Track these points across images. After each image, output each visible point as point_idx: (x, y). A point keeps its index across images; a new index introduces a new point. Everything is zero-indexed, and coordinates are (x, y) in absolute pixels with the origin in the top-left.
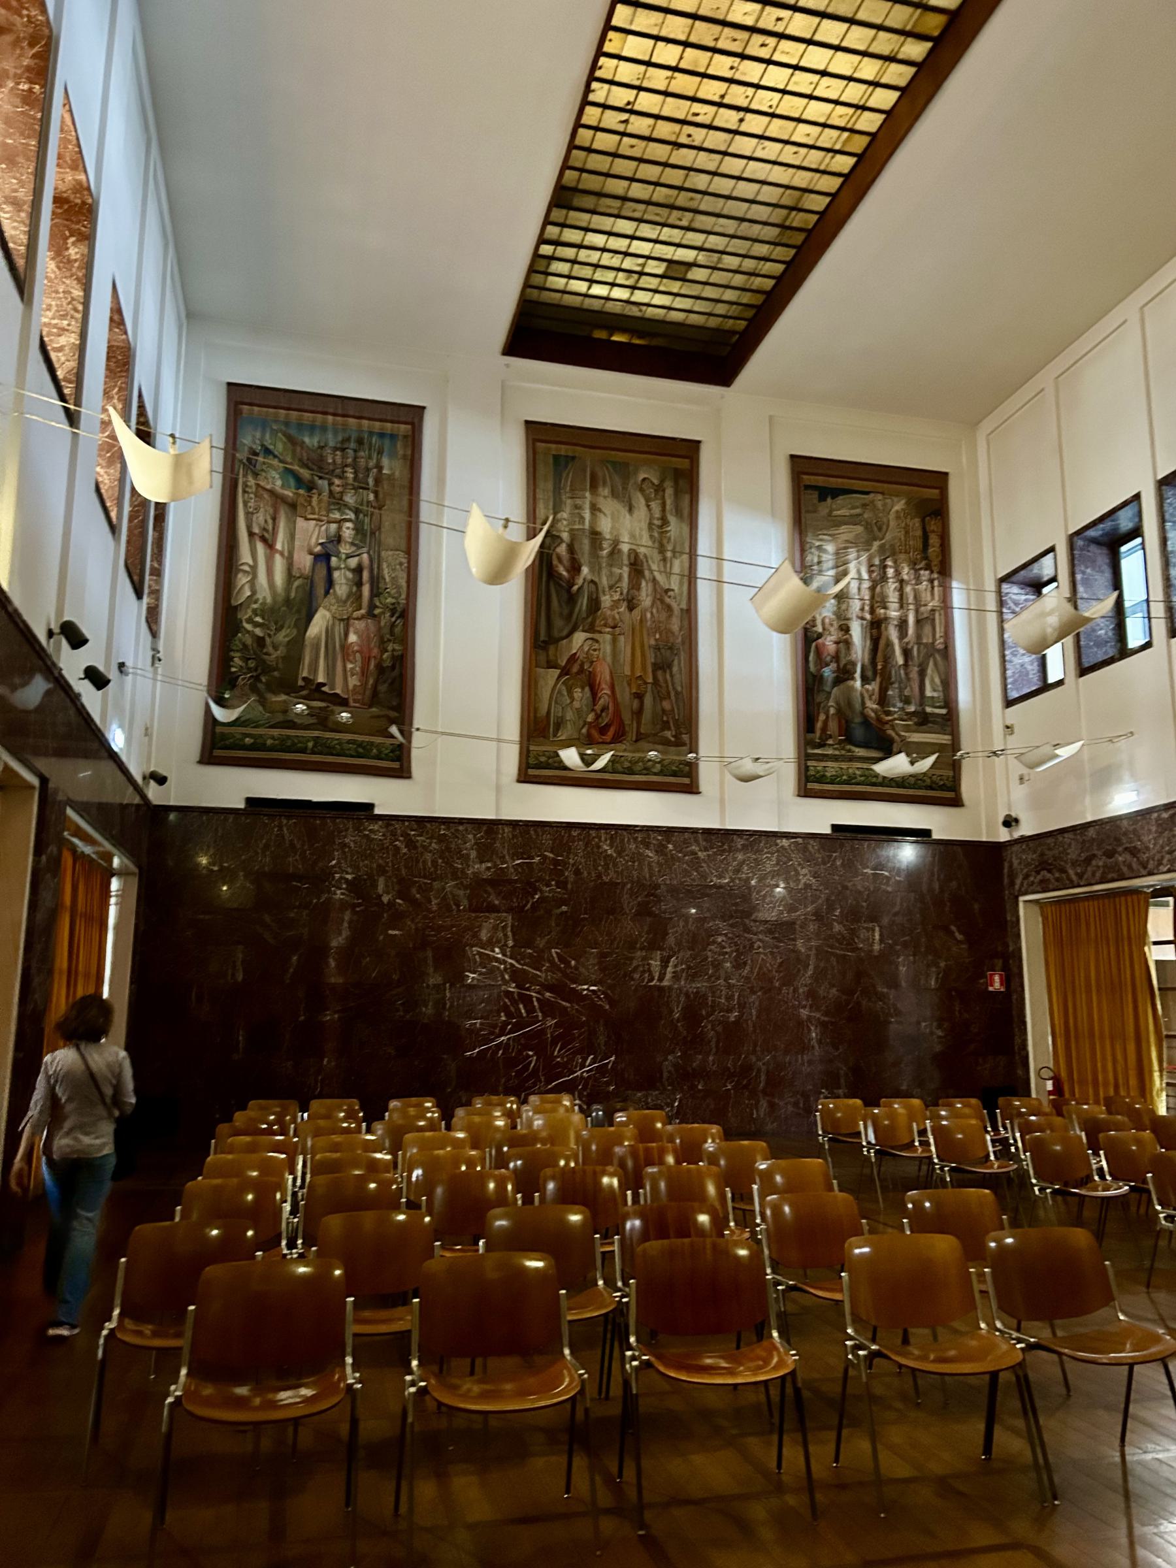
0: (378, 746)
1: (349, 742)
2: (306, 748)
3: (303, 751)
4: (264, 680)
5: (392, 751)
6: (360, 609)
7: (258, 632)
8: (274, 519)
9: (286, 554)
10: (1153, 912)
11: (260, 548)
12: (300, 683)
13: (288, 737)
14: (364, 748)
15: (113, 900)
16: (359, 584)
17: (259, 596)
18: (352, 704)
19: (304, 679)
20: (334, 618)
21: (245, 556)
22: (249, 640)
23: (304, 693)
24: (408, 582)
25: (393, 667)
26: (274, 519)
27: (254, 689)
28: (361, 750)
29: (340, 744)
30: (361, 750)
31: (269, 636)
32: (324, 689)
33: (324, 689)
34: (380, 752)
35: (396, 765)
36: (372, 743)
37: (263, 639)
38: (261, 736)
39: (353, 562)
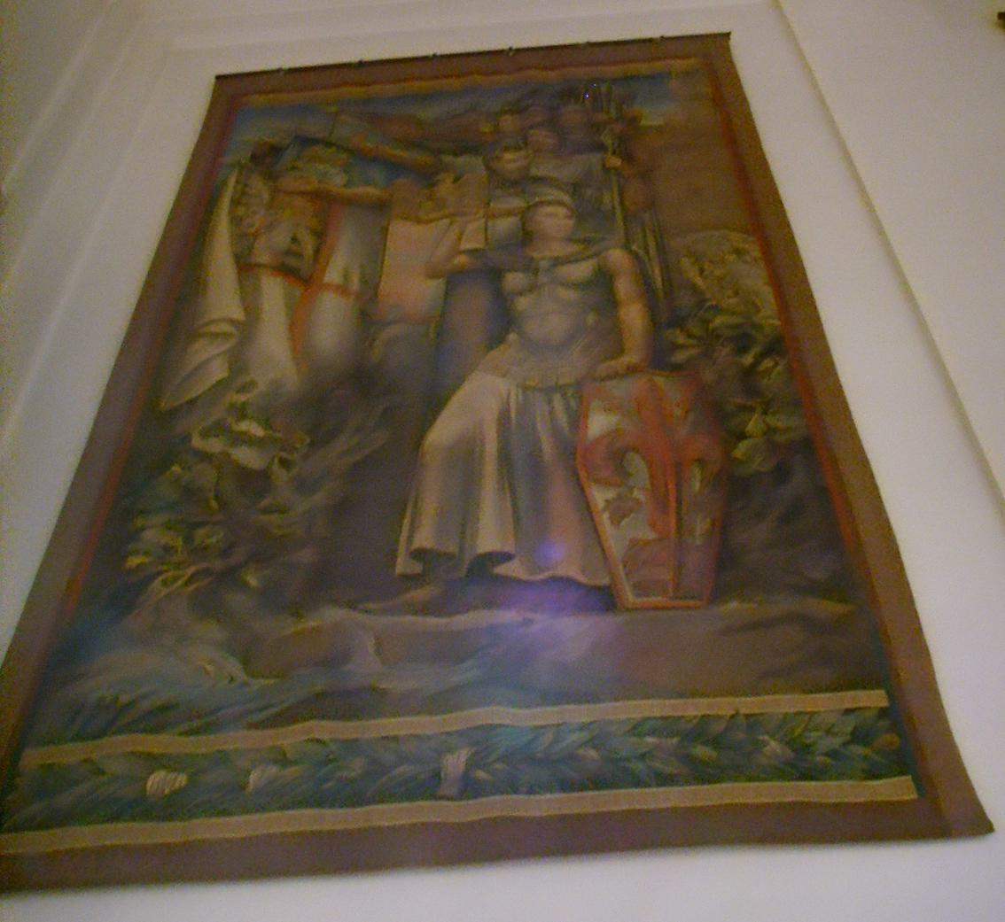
0: (784, 727)
1: (637, 729)
2: (436, 776)
3: (428, 787)
4: (253, 580)
5: (859, 736)
6: (620, 351)
7: (248, 457)
8: (321, 235)
9: (355, 284)
10: (882, 692)
11: (273, 291)
12: (403, 565)
13: (352, 746)
14: (715, 742)
15: (645, 599)
16: (610, 303)
17: (262, 378)
18: (630, 597)
19: (419, 554)
20: (525, 389)
21: (223, 297)
22: (206, 476)
23: (420, 594)
24: (776, 282)
25: (781, 473)
26: (321, 235)
27: (206, 606)
28: (702, 751)
29: (594, 742)
30: (702, 751)
31: (285, 463)
32: (502, 569)
33: (502, 569)
34: (804, 749)
35: (896, 789)
36: (753, 722)
37: (264, 475)
38: (222, 758)
39: (582, 270)
